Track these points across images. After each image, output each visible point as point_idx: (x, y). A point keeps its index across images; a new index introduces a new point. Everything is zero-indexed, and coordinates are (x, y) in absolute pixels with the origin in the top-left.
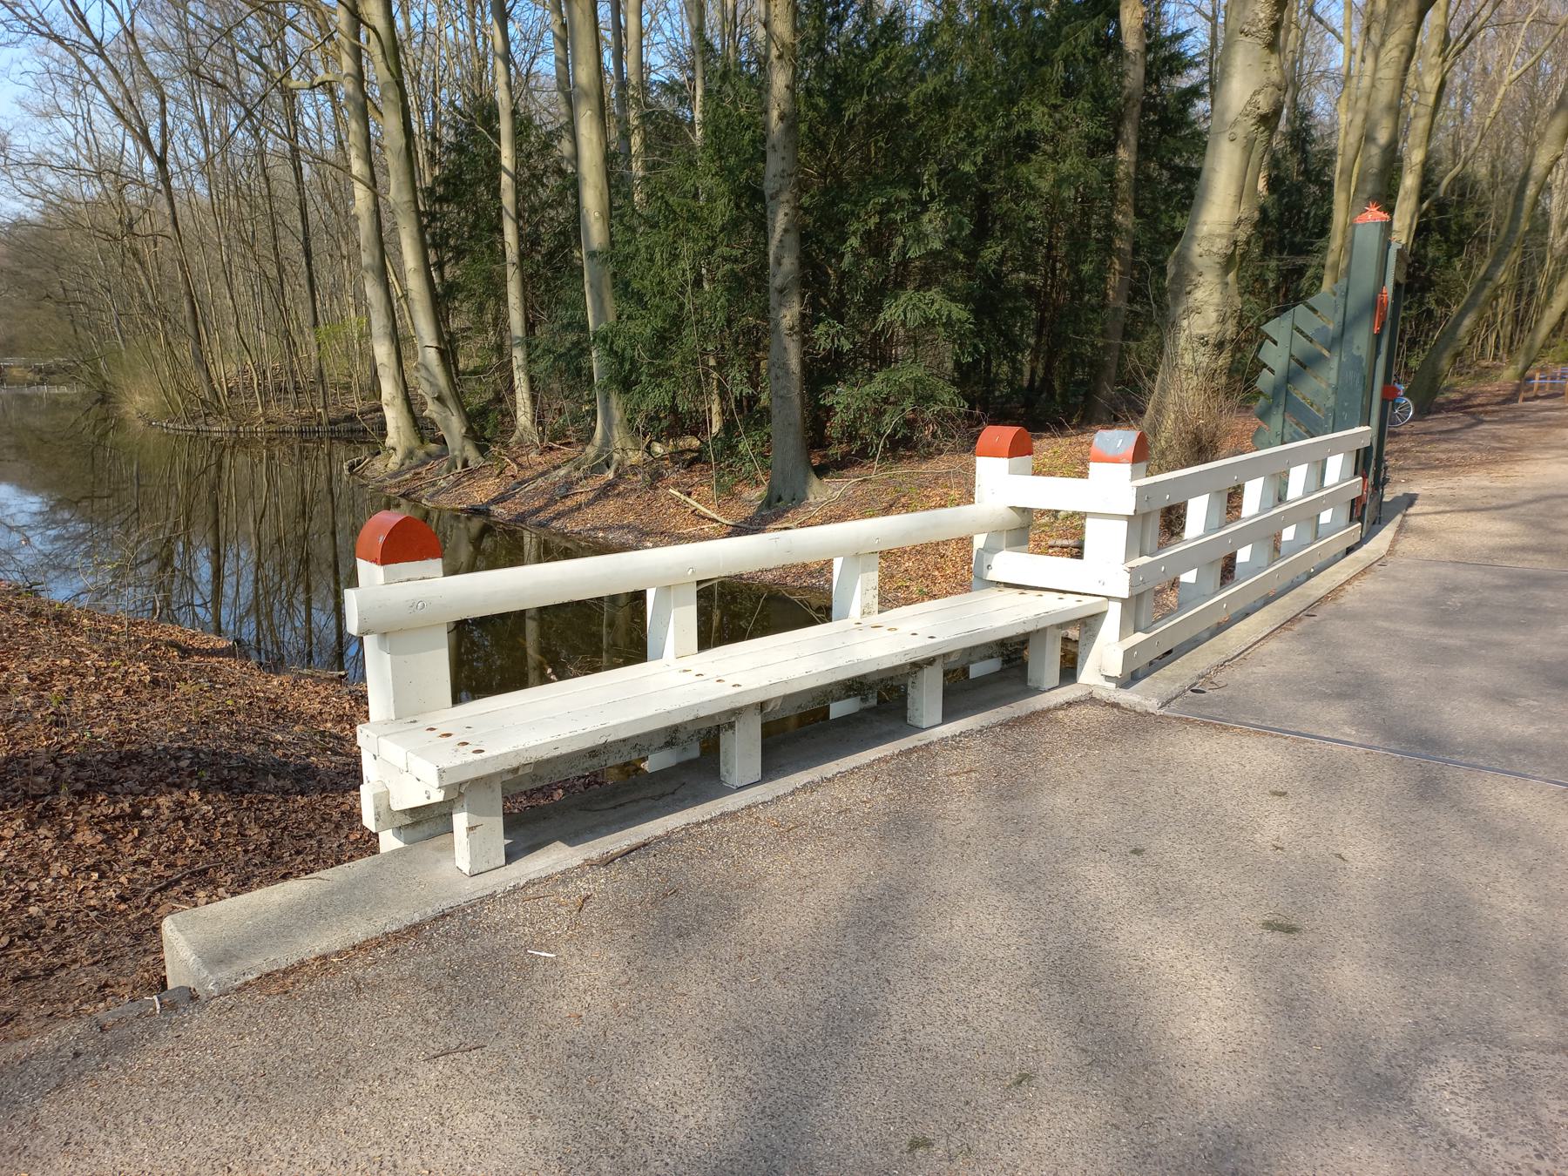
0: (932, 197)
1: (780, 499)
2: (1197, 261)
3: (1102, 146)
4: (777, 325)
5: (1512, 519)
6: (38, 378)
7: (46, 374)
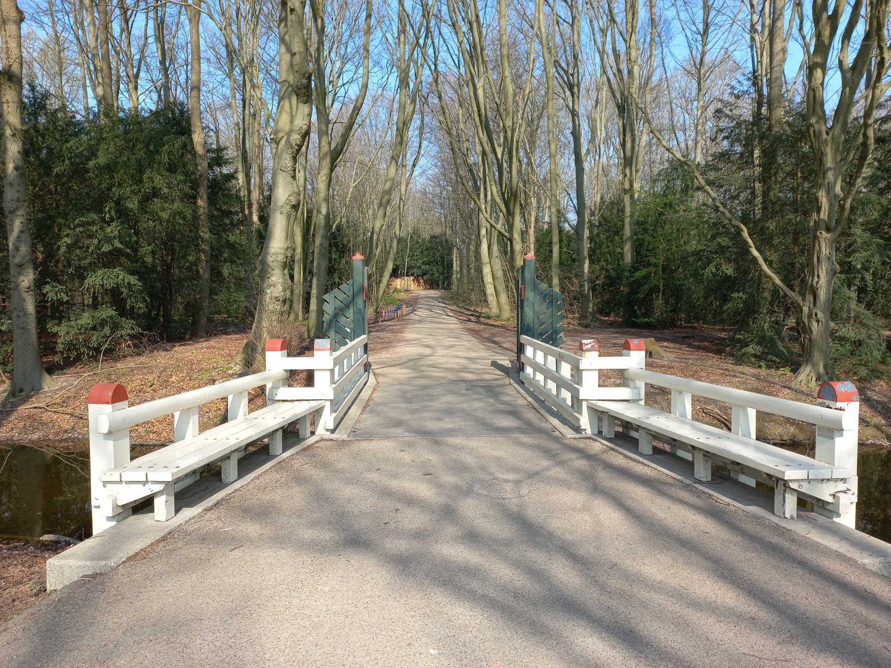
0: (112, 219)
1: (21, 391)
2: (271, 264)
3: (192, 198)
4: (18, 285)
5: (407, 368)
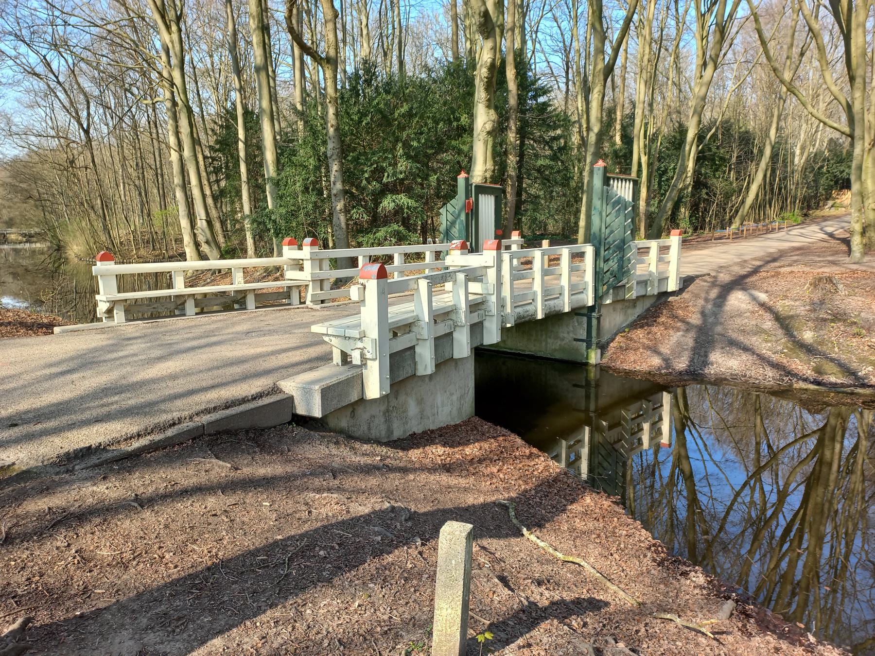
6: (24, 239)
7: (29, 238)
